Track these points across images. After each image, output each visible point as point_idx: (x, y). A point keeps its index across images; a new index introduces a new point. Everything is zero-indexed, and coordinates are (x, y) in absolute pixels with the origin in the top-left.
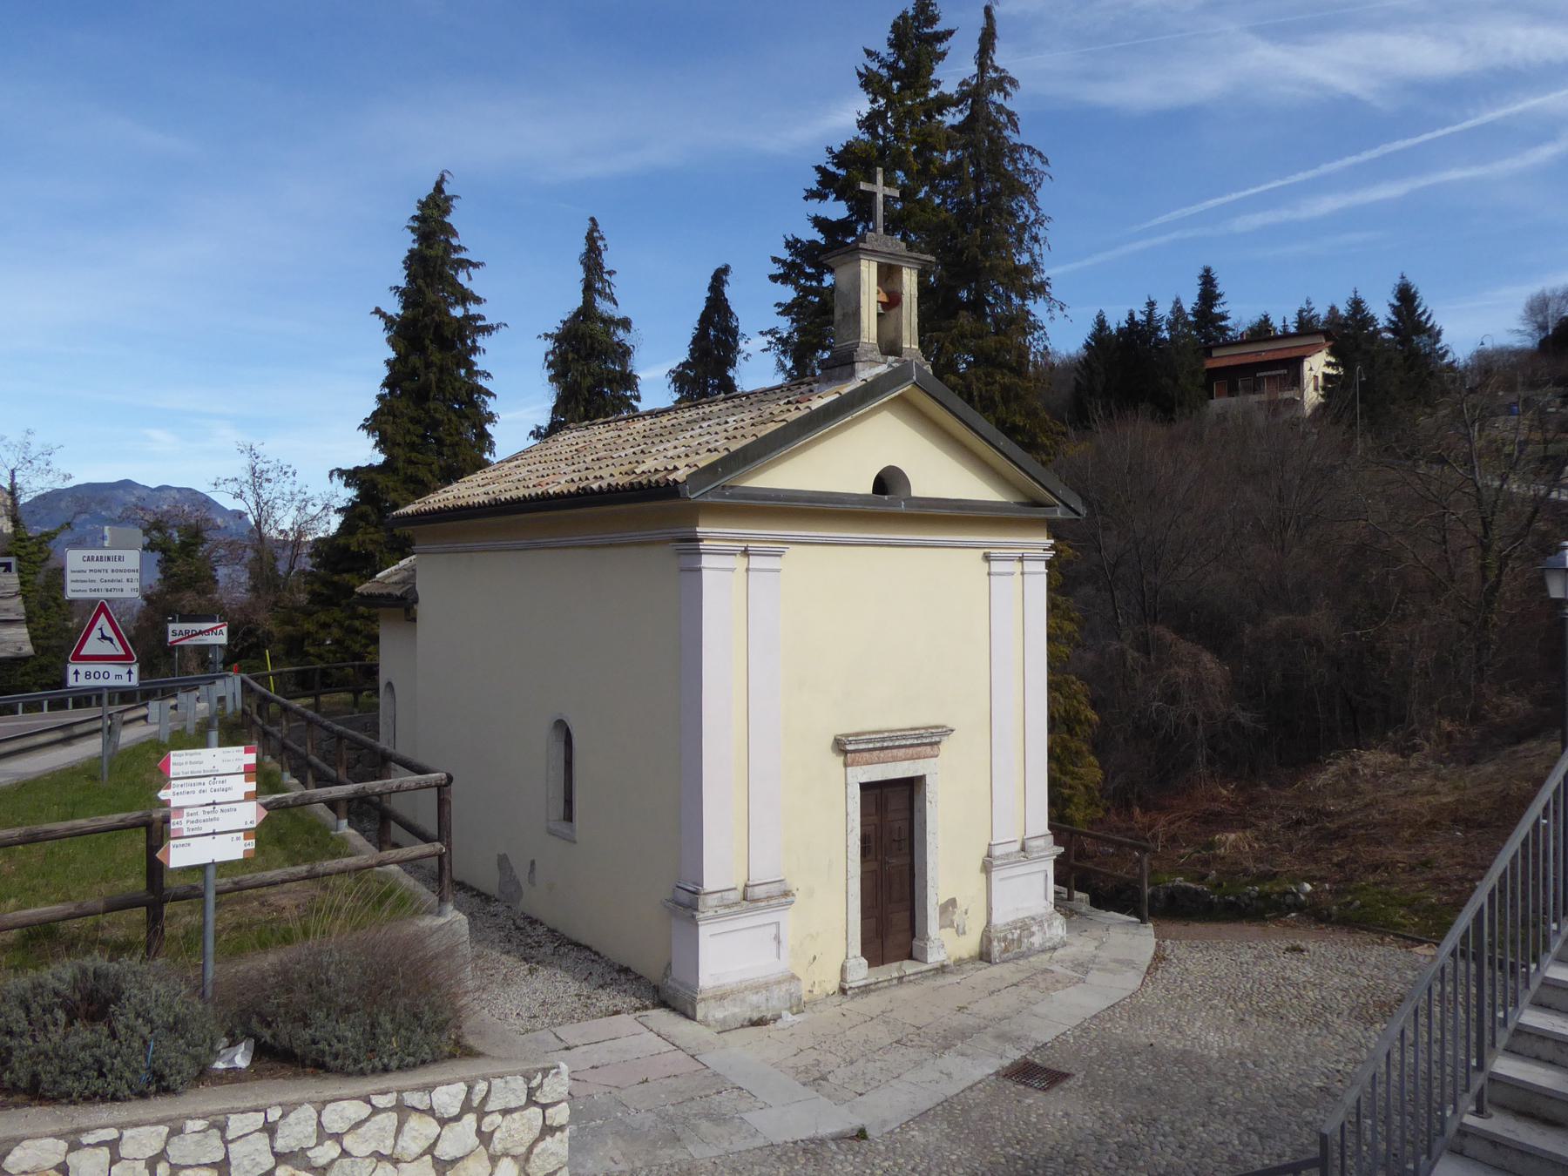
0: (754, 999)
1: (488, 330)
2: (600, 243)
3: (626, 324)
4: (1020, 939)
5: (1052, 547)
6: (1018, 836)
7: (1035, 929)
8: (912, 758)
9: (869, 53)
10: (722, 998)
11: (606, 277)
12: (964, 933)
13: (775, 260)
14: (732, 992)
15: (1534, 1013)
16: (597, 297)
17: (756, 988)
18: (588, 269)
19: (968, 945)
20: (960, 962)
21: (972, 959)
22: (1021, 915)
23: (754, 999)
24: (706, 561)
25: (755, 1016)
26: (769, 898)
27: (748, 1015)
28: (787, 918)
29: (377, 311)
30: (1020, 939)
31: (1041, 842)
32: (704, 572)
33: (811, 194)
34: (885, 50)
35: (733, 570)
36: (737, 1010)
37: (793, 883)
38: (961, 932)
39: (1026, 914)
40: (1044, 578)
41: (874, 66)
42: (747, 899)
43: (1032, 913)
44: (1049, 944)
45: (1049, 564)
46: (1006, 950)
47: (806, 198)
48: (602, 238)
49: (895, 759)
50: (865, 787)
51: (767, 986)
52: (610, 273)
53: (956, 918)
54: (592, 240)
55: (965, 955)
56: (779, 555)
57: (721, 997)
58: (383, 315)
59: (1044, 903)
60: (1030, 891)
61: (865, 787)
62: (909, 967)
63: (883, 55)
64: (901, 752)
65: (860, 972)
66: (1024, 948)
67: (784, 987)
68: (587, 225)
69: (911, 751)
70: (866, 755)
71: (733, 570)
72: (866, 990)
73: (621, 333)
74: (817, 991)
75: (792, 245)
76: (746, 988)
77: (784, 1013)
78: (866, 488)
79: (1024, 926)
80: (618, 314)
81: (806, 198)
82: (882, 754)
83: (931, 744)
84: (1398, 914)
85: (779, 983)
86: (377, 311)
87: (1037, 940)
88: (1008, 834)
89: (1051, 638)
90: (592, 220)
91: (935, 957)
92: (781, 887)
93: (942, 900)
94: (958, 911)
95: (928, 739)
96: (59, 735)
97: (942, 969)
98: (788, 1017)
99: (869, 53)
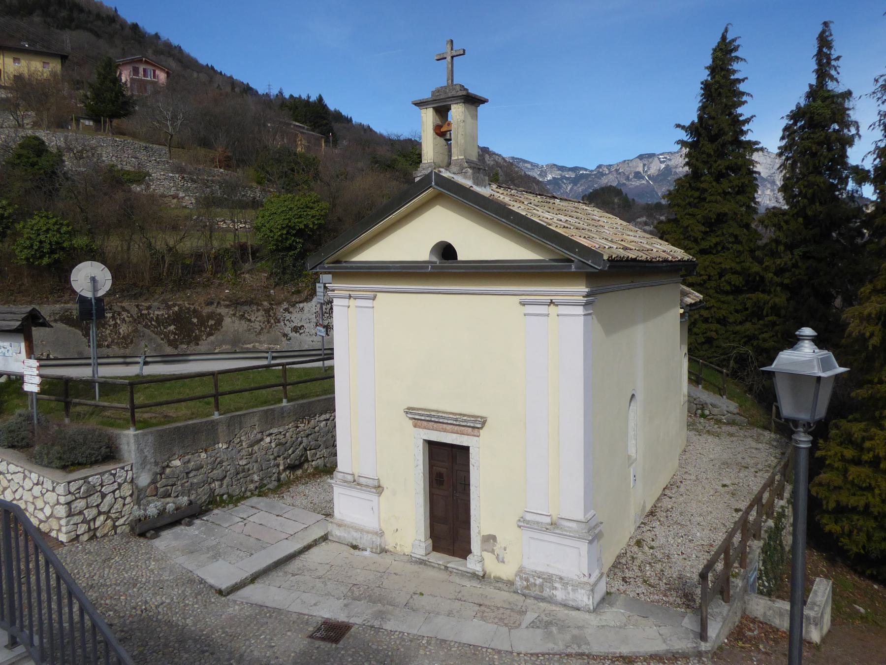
0: (355, 534)
1: (747, 121)
4: (541, 586)
10: (340, 526)
11: (833, 63)
12: (503, 562)
14: (345, 526)
15: (126, 455)
17: (361, 530)
18: (819, 63)
20: (498, 580)
22: (551, 571)
23: (355, 534)
25: (354, 543)
26: (367, 486)
29: (678, 126)
30: (541, 586)
31: (574, 525)
38: (500, 560)
43: (563, 575)
44: (571, 603)
46: (527, 587)
47: (483, 101)
49: (445, 431)
52: (838, 58)
54: (824, 42)
55: (504, 576)
58: (683, 127)
62: (455, 563)
67: (370, 536)
69: (456, 428)
70: (424, 423)
71: (548, 315)
72: (422, 562)
76: (352, 527)
77: (369, 550)
79: (549, 579)
81: (483, 101)
82: (435, 425)
83: (473, 428)
84: (121, 422)
85: (368, 532)
86: (678, 126)
89: (689, 372)
90: (826, 24)
91: (472, 564)
95: (476, 424)
96: (121, 360)
97: (474, 576)
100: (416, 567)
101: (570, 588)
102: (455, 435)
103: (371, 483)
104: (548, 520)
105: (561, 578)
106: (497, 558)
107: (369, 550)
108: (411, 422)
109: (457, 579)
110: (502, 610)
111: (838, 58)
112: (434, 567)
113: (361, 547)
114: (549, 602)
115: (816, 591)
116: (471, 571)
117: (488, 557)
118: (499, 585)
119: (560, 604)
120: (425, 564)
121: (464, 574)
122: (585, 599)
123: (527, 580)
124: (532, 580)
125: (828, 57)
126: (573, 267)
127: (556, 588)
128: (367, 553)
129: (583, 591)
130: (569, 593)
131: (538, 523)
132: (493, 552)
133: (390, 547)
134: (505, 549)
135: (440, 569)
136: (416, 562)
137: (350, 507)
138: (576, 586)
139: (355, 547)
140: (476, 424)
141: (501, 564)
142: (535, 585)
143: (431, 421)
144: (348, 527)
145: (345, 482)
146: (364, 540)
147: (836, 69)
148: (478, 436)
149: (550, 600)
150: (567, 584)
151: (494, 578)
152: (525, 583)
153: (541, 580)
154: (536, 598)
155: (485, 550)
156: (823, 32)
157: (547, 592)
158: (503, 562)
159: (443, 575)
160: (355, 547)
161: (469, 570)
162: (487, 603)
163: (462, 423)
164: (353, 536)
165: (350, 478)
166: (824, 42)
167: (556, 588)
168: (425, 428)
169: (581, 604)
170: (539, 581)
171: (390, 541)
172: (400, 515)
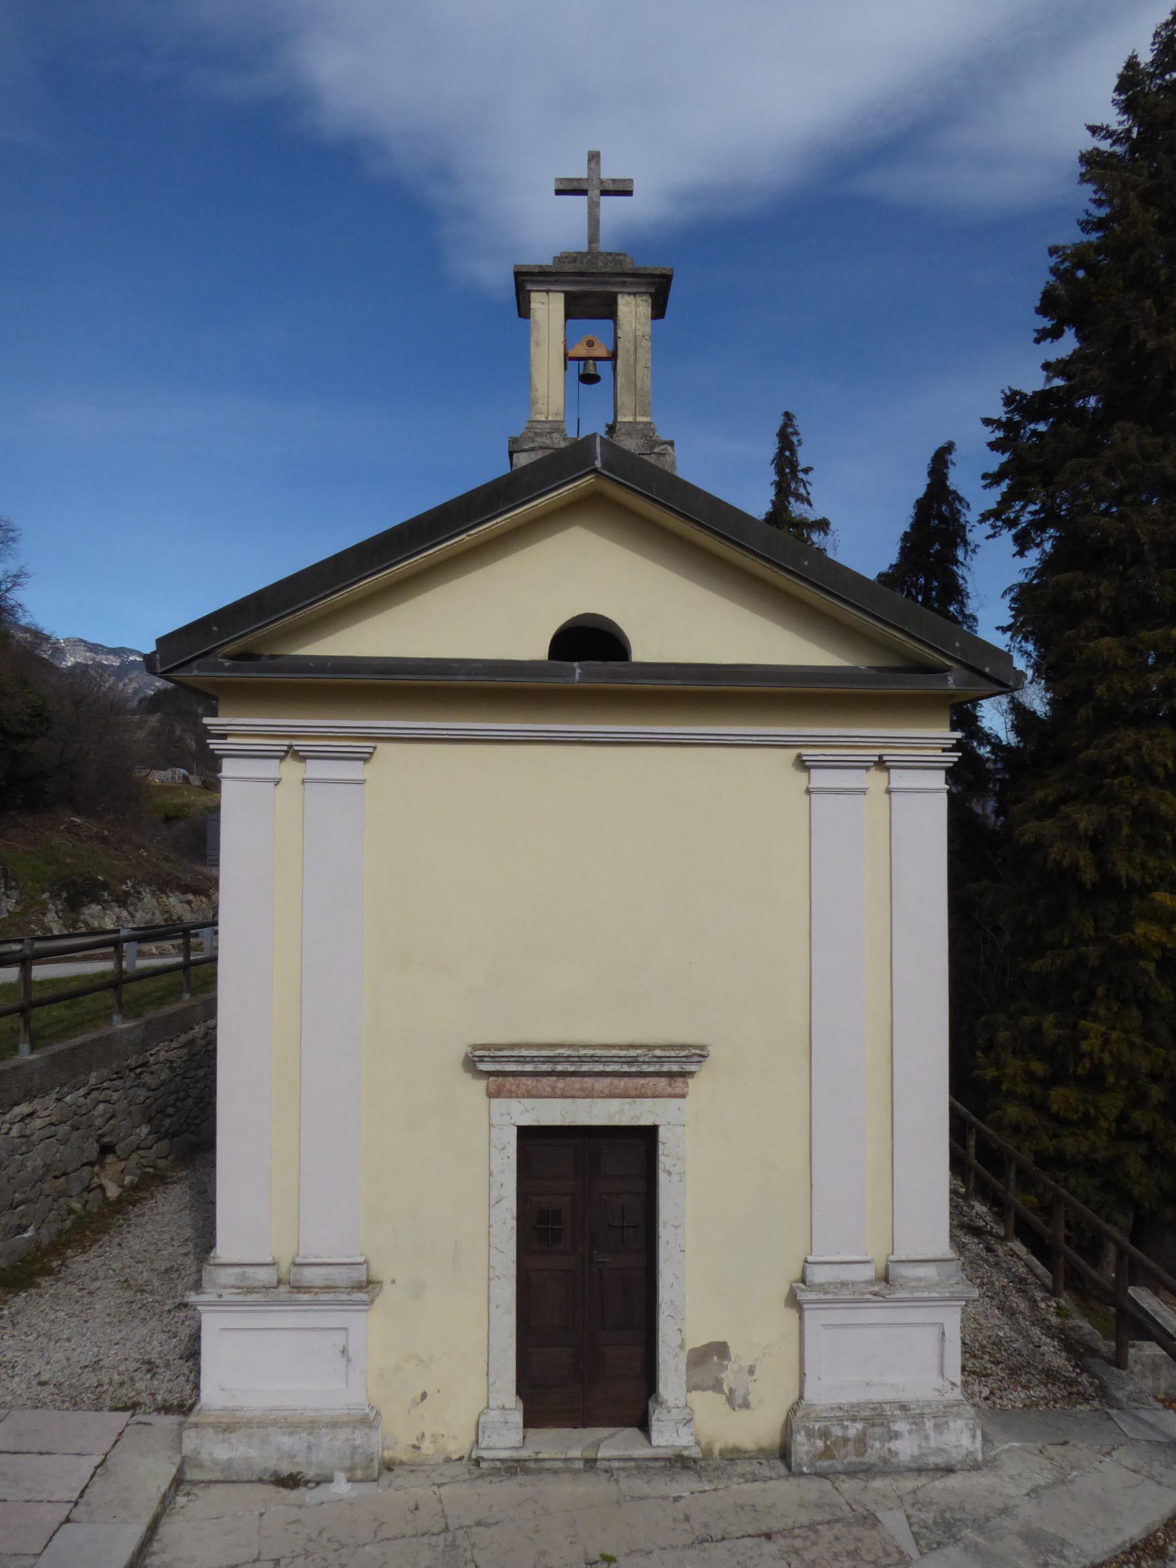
0: (286, 1442)
2: (795, 439)
3: (823, 525)
4: (861, 1442)
5: (958, 746)
6: (877, 1253)
7: (901, 1426)
8: (625, 1095)
9: (1094, 130)
11: (801, 475)
12: (746, 1405)
13: (987, 422)
14: (249, 1424)
16: (792, 500)
17: (290, 1425)
18: (780, 471)
19: (757, 1427)
20: (734, 1455)
21: (763, 1454)
22: (875, 1396)
23: (286, 1442)
24: (229, 767)
25: (286, 1469)
27: (272, 1464)
28: (371, 1328)
30: (861, 1442)
31: (929, 1272)
32: (225, 786)
33: (1043, 335)
34: (1114, 119)
35: (863, 792)
36: (253, 1453)
37: (379, 1270)
38: (738, 1402)
39: (889, 1396)
40: (940, 804)
41: (1105, 145)
42: (290, 1287)
43: (904, 1397)
44: (933, 1460)
45: (952, 774)
46: (827, 1453)
47: (1037, 341)
48: (796, 433)
49: (589, 1094)
50: (524, 1133)
51: (312, 1426)
52: (807, 471)
53: (729, 1378)
54: (786, 441)
55: (748, 1442)
56: (366, 758)
57: (228, 1426)
59: (938, 1382)
60: (907, 1359)
61: (524, 1133)
62: (615, 1443)
63: (1114, 126)
64: (602, 1084)
65: (507, 1434)
66: (871, 1457)
68: (779, 421)
69: (623, 1083)
70: (529, 1082)
71: (863, 792)
72: (513, 1468)
73: (816, 537)
74: (427, 1447)
75: (1012, 399)
76: (275, 1423)
78: (537, 648)
79: (877, 1418)
80: (812, 515)
81: (1037, 341)
82: (561, 1084)
83: (671, 1075)
85: (334, 1425)
87: (906, 1448)
88: (851, 1242)
90: (787, 415)
91: (667, 1435)
92: (360, 1275)
93: (697, 1340)
94: (732, 1367)
97: (680, 1463)
98: (341, 1487)
99: (1094, 130)
100: (509, 1489)
101: (929, 1424)
102: (616, 1102)
103: (339, 1276)
104: (868, 1272)
105: (904, 1407)
106: (730, 1400)
107: (340, 1477)
108: (481, 1085)
109: (639, 1485)
110: (826, 1533)
111: (807, 471)
112: (555, 1472)
113: (310, 1474)
114: (884, 1474)
115: (1153, 1311)
116: (669, 1453)
117: (707, 1405)
118: (742, 1467)
119: (910, 1470)
120: (527, 1471)
121: (643, 1467)
122: (966, 1441)
123: (825, 1434)
124: (837, 1431)
125: (793, 465)
126: (951, 680)
127: (896, 1435)
128: (341, 1487)
129: (960, 1423)
130: (927, 1438)
131: (844, 1284)
132: (717, 1386)
133: (399, 1453)
134: (751, 1371)
135: (576, 1472)
136: (494, 1472)
137: (252, 1366)
138: (943, 1415)
139: (290, 1482)
140: (670, 1067)
141: (744, 1412)
142: (845, 1440)
143: (574, 1074)
144: (262, 1425)
145: (250, 1290)
146: (328, 1449)
147: (805, 487)
148: (683, 1096)
149: (886, 1468)
150: (922, 1415)
151: (721, 1452)
152: (820, 1444)
153: (859, 1425)
154: (852, 1472)
155: (696, 1388)
156: (784, 427)
157: (876, 1450)
158: (746, 1405)
159: (594, 1488)
160: (290, 1482)
161: (661, 1453)
162: (776, 1525)
163: (645, 1068)
164: (284, 1450)
165: (264, 1276)
166: (786, 441)
167: (896, 1435)
168: (529, 1095)
169: (956, 1455)
170: (854, 1429)
171: (398, 1435)
172: (442, 1350)
